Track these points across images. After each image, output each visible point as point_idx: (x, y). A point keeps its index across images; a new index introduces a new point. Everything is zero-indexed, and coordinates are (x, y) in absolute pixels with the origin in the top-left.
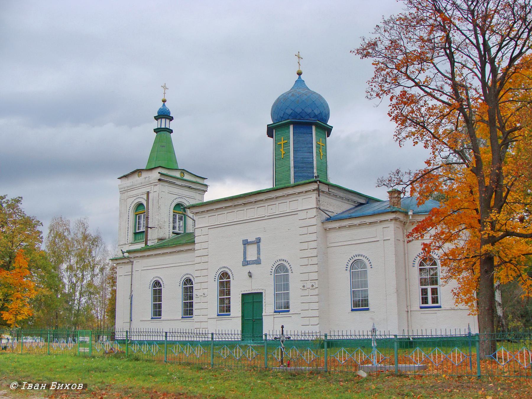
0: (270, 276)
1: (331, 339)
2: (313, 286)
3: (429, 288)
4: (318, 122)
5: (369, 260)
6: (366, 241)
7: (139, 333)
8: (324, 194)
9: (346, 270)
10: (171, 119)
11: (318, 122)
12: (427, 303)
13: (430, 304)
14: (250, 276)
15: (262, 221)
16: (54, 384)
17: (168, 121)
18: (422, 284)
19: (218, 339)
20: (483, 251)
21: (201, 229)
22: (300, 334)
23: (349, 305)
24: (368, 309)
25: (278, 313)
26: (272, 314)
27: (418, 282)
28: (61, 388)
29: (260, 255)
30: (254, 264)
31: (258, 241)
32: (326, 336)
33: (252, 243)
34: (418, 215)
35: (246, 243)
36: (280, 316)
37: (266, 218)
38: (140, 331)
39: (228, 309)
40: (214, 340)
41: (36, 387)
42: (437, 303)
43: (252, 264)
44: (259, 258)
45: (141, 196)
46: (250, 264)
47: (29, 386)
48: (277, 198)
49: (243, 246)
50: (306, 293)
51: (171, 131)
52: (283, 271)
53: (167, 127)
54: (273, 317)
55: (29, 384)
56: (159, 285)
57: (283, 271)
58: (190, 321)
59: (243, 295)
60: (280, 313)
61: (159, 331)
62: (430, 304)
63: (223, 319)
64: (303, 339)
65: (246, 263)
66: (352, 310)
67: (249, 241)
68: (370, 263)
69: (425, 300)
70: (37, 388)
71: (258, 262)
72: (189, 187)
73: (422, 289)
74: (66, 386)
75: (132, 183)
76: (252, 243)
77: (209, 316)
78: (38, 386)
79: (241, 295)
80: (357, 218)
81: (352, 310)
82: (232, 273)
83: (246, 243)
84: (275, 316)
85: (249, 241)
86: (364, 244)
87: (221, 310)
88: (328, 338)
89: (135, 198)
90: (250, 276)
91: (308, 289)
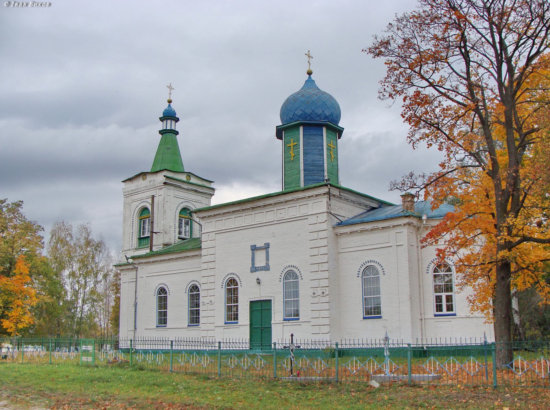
2: (323, 293)
3: (444, 295)
5: (382, 267)
9: (358, 276)
10: (177, 120)
12: (441, 310)
13: (445, 311)
14: (259, 283)
17: (173, 122)
18: (436, 291)
19: (225, 348)
21: (208, 234)
22: (310, 343)
23: (360, 313)
24: (380, 317)
25: (288, 321)
26: (281, 322)
27: (432, 289)
30: (262, 270)
31: (267, 247)
32: (337, 345)
35: (254, 249)
39: (236, 317)
40: (222, 349)
42: (452, 310)
43: (261, 270)
44: (267, 264)
45: (146, 200)
46: (258, 270)
49: (251, 252)
50: (316, 300)
51: (177, 133)
52: (293, 277)
53: (173, 128)
54: (282, 325)
56: (164, 292)
57: (293, 277)
60: (290, 321)
61: (164, 340)
62: (445, 311)
64: (313, 348)
65: (254, 269)
66: (364, 318)
69: (439, 308)
71: (266, 268)
72: (196, 191)
73: (436, 296)
75: (136, 187)
77: (216, 325)
79: (249, 303)
81: (364, 318)
82: (240, 280)
83: (254, 249)
84: (284, 324)
87: (229, 318)
88: (340, 347)
89: (140, 202)
90: (259, 283)
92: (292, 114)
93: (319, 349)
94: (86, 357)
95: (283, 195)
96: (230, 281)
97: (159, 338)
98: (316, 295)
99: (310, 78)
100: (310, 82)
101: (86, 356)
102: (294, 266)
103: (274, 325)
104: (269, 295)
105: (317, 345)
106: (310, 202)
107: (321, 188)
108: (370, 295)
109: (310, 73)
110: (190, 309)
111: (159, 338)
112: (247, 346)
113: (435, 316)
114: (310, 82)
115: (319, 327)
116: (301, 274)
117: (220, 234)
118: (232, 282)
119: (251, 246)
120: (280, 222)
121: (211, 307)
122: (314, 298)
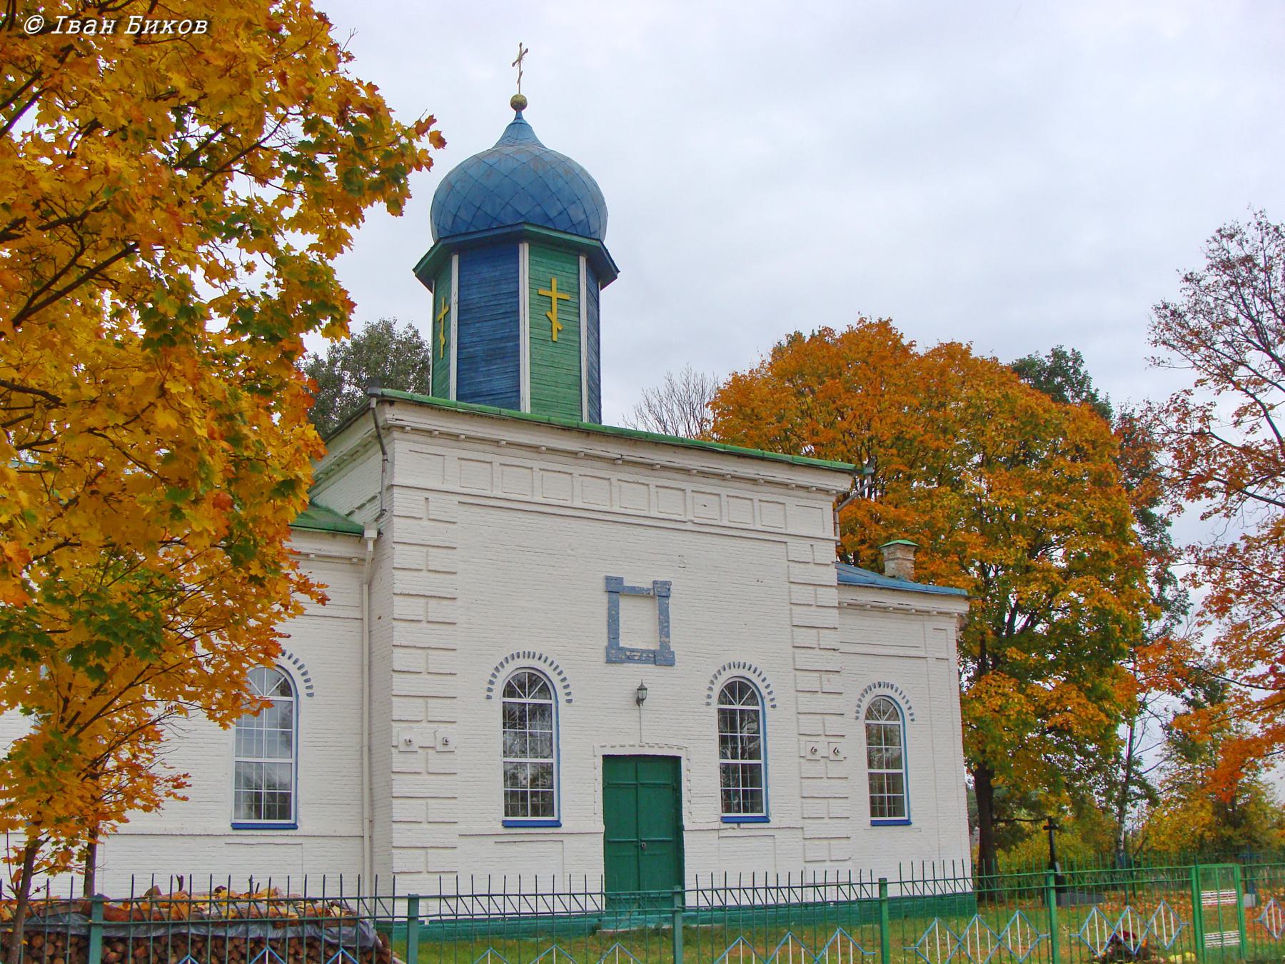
0: (706, 708)
1: (905, 894)
2: (814, 751)
4: (527, 227)
5: (907, 702)
6: (901, 652)
7: (371, 892)
8: (406, 436)
9: (857, 718)
11: (527, 227)
14: (639, 701)
15: (520, 514)
16: (136, 20)
20: (95, 638)
21: (427, 494)
26: (716, 826)
28: (152, 29)
29: (668, 636)
30: (647, 661)
31: (660, 593)
32: (883, 884)
33: (636, 593)
34: (300, 531)
35: (615, 588)
36: (738, 833)
37: (689, 526)
38: (949, 875)
41: (89, 29)
43: (640, 661)
44: (665, 646)
46: (630, 659)
47: (72, 26)
48: (754, 481)
49: (604, 598)
50: (816, 770)
54: (715, 834)
55: (72, 22)
57: (741, 698)
58: (250, 841)
59: (676, 761)
60: (742, 825)
61: (855, 879)
63: (540, 838)
64: (745, 902)
65: (617, 655)
67: (626, 584)
68: (491, 682)
70: (93, 31)
71: (662, 657)
74: (166, 26)
76: (636, 593)
77: (462, 827)
78: (94, 26)
79: (600, 761)
80: (883, 591)
83: (615, 588)
84: (722, 834)
85: (626, 584)
86: (895, 659)
87: (877, 808)
88: (893, 891)
90: (639, 701)
91: (822, 760)
92: (559, 207)
93: (825, 903)
94: (1218, 934)
95: (735, 459)
96: (731, 687)
97: (917, 867)
98: (817, 756)
99: (519, 117)
100: (518, 128)
101: (1215, 930)
102: (508, 655)
103: (690, 833)
104: (674, 742)
105: (579, 898)
106: (791, 502)
107: (806, 470)
108: (879, 768)
109: (519, 105)
110: (903, 771)
111: (917, 867)
112: (596, 904)
113: (236, 827)
114: (518, 128)
115: (825, 842)
116: (566, 687)
117: (477, 509)
118: (738, 690)
119: (608, 579)
120: (703, 529)
121: (437, 762)
122: (813, 763)
